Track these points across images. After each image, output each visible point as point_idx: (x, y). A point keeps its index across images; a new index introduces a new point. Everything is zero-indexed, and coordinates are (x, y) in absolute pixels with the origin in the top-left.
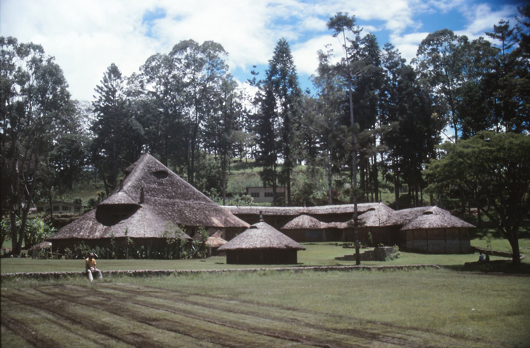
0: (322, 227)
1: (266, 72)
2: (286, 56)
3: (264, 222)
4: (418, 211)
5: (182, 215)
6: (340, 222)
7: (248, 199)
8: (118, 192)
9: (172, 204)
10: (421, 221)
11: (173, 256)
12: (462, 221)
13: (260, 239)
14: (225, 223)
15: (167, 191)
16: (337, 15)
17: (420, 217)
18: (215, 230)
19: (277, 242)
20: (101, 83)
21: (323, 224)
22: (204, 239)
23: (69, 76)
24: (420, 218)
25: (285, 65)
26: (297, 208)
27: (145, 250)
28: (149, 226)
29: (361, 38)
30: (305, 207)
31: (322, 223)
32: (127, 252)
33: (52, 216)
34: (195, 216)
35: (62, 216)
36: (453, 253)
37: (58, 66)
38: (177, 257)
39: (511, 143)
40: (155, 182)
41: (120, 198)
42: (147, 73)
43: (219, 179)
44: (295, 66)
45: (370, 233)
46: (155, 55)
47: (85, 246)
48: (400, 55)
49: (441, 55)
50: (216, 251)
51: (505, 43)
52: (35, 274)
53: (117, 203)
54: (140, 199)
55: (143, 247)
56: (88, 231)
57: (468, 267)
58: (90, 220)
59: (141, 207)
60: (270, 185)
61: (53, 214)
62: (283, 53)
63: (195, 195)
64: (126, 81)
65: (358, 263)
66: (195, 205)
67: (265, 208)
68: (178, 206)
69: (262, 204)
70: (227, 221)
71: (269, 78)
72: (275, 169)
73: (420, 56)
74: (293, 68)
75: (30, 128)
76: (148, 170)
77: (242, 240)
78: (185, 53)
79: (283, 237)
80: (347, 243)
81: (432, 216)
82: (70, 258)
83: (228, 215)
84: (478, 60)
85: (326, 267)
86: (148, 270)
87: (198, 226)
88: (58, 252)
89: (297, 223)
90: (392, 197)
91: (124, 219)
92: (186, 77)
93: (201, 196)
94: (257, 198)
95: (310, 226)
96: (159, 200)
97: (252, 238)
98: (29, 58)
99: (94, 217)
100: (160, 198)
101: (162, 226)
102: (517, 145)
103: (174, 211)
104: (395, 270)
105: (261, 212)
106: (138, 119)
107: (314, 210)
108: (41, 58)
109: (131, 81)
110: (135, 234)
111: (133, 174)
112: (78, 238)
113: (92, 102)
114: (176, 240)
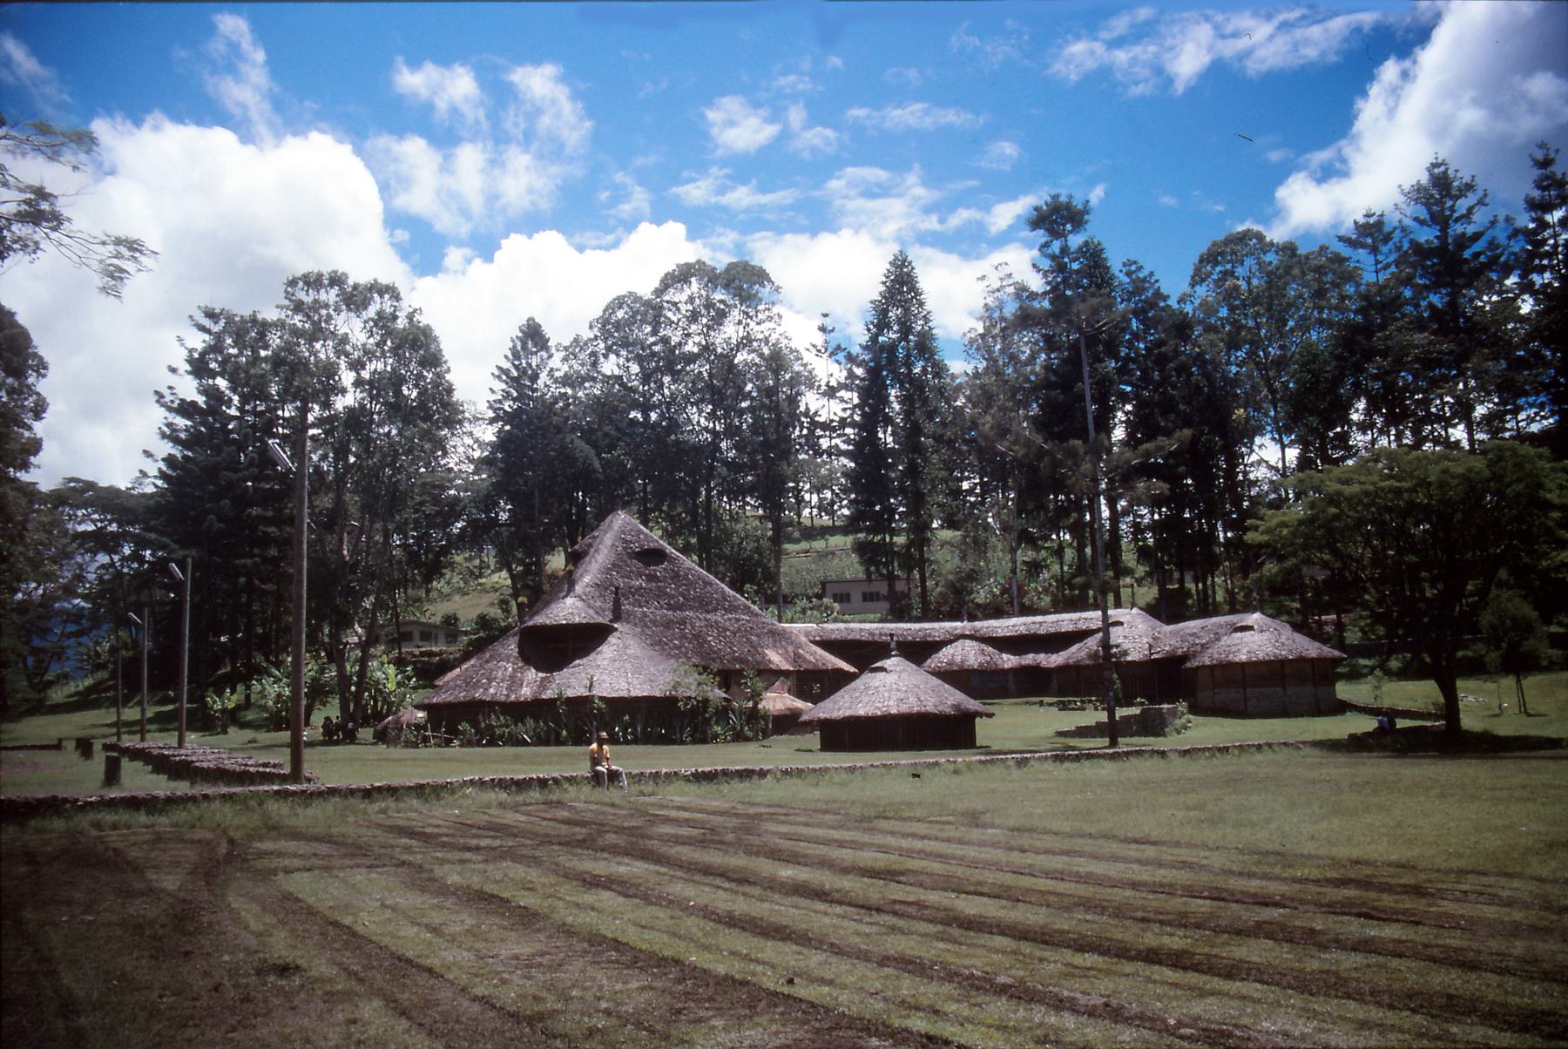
4: (1220, 626)
7: (827, 608)
11: (692, 736)
12: (1317, 644)
13: (895, 695)
15: (666, 594)
16: (1049, 200)
22: (756, 696)
23: (449, 346)
24: (1226, 640)
25: (907, 310)
26: (948, 625)
27: (633, 724)
28: (638, 671)
29: (1072, 250)
30: (965, 623)
33: (400, 653)
35: (422, 654)
36: (1302, 716)
38: (702, 737)
39: (1445, 471)
40: (640, 575)
42: (606, 335)
43: (758, 563)
45: (1115, 676)
48: (1157, 285)
49: (1243, 285)
50: (788, 723)
51: (1380, 258)
57: (1356, 744)
60: (882, 575)
61: (403, 650)
62: (902, 284)
64: (558, 356)
65: (1113, 743)
67: (880, 625)
68: (693, 625)
69: (862, 616)
71: (874, 339)
73: (1198, 288)
74: (924, 317)
76: (625, 549)
78: (688, 292)
79: (946, 690)
82: (469, 743)
84: (1320, 294)
87: (737, 671)
88: (445, 733)
90: (1149, 593)
91: (581, 657)
92: (690, 342)
94: (845, 605)
95: (981, 664)
97: (878, 692)
98: (371, 312)
100: (652, 610)
101: (665, 670)
102: (1458, 476)
103: (684, 637)
104: (1213, 756)
105: (892, 635)
106: (588, 434)
109: (571, 352)
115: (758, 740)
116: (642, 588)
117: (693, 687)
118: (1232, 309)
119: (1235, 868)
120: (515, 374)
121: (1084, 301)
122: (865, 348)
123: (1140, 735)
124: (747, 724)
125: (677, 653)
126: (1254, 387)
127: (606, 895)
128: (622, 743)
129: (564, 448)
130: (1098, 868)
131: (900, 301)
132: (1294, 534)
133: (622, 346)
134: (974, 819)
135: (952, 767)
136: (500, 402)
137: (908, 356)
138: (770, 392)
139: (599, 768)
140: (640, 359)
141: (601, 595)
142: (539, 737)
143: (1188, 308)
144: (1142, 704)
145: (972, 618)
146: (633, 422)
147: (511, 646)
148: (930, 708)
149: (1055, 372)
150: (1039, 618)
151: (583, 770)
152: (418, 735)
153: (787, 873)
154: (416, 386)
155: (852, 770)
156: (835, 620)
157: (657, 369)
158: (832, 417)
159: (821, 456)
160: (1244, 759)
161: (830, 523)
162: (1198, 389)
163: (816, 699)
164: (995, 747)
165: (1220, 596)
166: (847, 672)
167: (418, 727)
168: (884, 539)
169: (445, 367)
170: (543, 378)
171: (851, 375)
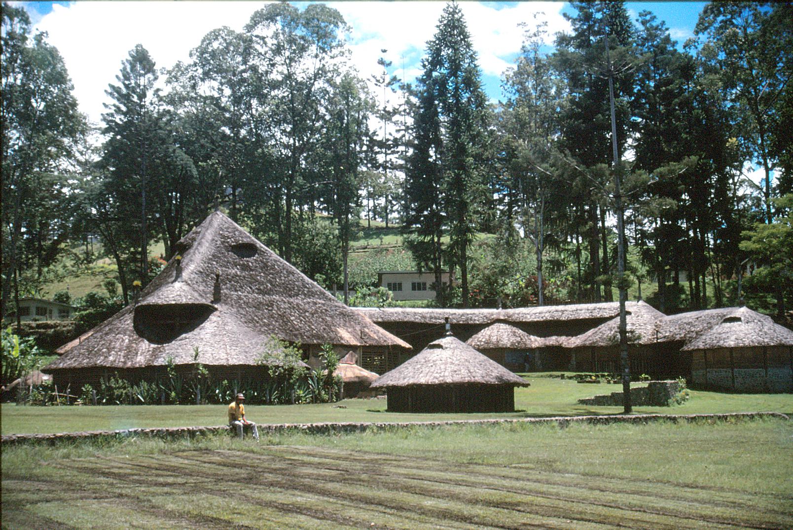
0: (533, 346)
1: (423, 62)
2: (460, 34)
3: (453, 338)
4: (712, 317)
5: (287, 324)
6: (567, 336)
7: (383, 295)
8: (172, 282)
9: (267, 305)
10: (720, 334)
14: (361, 338)
15: (257, 281)
17: (717, 327)
18: (346, 352)
19: (481, 372)
20: (117, 80)
21: (536, 340)
22: (331, 366)
24: (717, 329)
25: (456, 50)
26: (486, 311)
28: (235, 343)
30: (500, 310)
31: (532, 337)
32: (198, 392)
34: (309, 326)
35: (38, 326)
36: (781, 392)
37: (57, 51)
40: (235, 264)
41: (178, 293)
42: (203, 62)
43: (326, 257)
44: (474, 53)
46: (220, 30)
47: (120, 381)
48: (667, 33)
52: (159, 431)
53: (173, 302)
54: (214, 294)
55: (226, 382)
56: (122, 354)
58: (125, 334)
59: (216, 309)
60: (431, 269)
61: (22, 323)
62: (454, 27)
63: (306, 287)
64: (163, 78)
66: (307, 306)
67: (430, 310)
70: (365, 335)
71: (429, 74)
72: (439, 240)
73: (700, 35)
74: (471, 56)
75: (8, 164)
76: (223, 243)
77: (418, 369)
79: (491, 365)
80: (583, 374)
81: (740, 325)
82: (92, 402)
83: (366, 324)
85: (606, 417)
86: (331, 423)
87: (314, 345)
88: (70, 393)
89: (487, 338)
90: (650, 288)
91: (186, 332)
93: (316, 289)
95: (513, 344)
96: (245, 296)
99: (131, 328)
101: (257, 344)
103: (272, 316)
105: (447, 319)
106: (186, 144)
107: (518, 314)
108: (24, 33)
109: (173, 78)
110: (211, 359)
111: (197, 248)
112: (105, 366)
113: (102, 114)
114: (285, 370)
115: (332, 402)
116: (237, 276)
117: (281, 358)
118: (730, 54)
119: (776, 508)
120: (124, 91)
121: (612, 48)
122: (422, 81)
123: (648, 404)
124: (324, 389)
125: (268, 330)
126: (745, 120)
127: (302, 518)
128: (221, 403)
129: (167, 156)
130: (670, 505)
131: (450, 42)
132: (782, 244)
133: (216, 72)
134: (549, 465)
135: (509, 426)
136: (112, 115)
137: (456, 89)
138: (339, 116)
139: (237, 422)
140: (232, 85)
141: (204, 281)
142: (152, 397)
143: (693, 53)
144: (646, 379)
145: (505, 307)
146: (224, 136)
147: (128, 322)
148: (479, 379)
149: (578, 105)
150: (561, 307)
151: (223, 423)
152: (46, 396)
153: (428, 503)
154: (43, 100)
155: (433, 426)
156: (390, 305)
157: (247, 94)
158: (388, 137)
159: (378, 168)
160: (740, 426)
161: (384, 224)
162: (699, 121)
163: (381, 371)
164: (530, 412)
165: (710, 292)
166: (404, 348)
167: (45, 388)
168: (433, 239)
169: (69, 84)
170: (150, 95)
171: (408, 102)
